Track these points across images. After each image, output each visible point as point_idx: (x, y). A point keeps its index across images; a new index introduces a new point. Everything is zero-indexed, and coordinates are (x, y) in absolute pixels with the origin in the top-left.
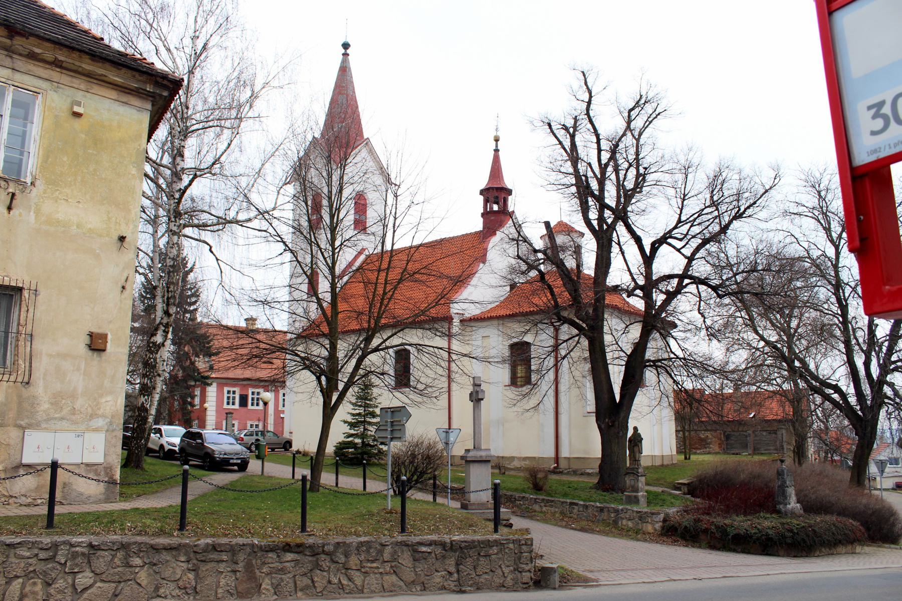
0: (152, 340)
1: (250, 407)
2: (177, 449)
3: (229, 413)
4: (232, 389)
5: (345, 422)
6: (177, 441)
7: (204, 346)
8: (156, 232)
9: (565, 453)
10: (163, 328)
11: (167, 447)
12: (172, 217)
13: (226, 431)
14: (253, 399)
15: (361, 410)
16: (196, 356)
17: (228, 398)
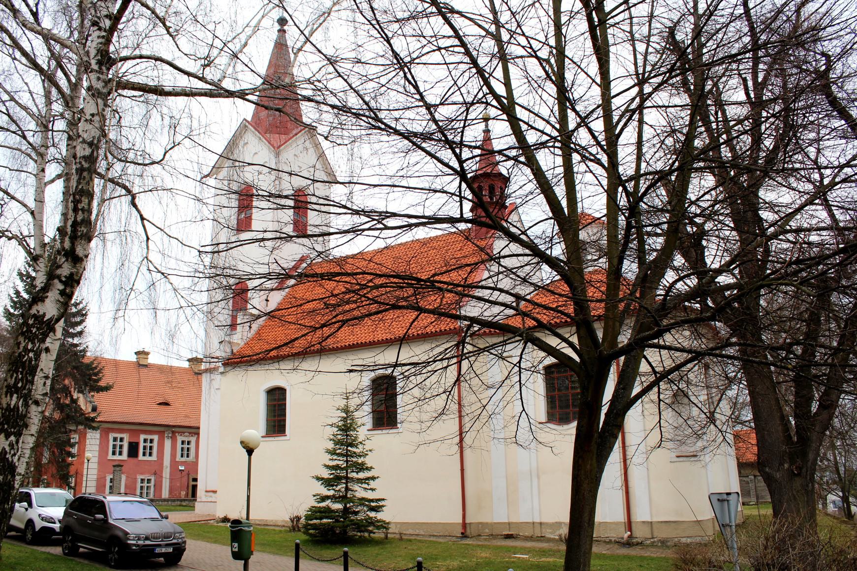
0: (33, 311)
1: (141, 457)
2: (57, 526)
3: (118, 466)
4: (119, 436)
5: (318, 479)
6: (58, 512)
7: (90, 379)
8: (43, 170)
9: (641, 514)
10: (61, 287)
11: (39, 524)
12: (93, 62)
13: (141, 496)
14: (145, 448)
15: (341, 463)
16: (79, 392)
17: (114, 446)
